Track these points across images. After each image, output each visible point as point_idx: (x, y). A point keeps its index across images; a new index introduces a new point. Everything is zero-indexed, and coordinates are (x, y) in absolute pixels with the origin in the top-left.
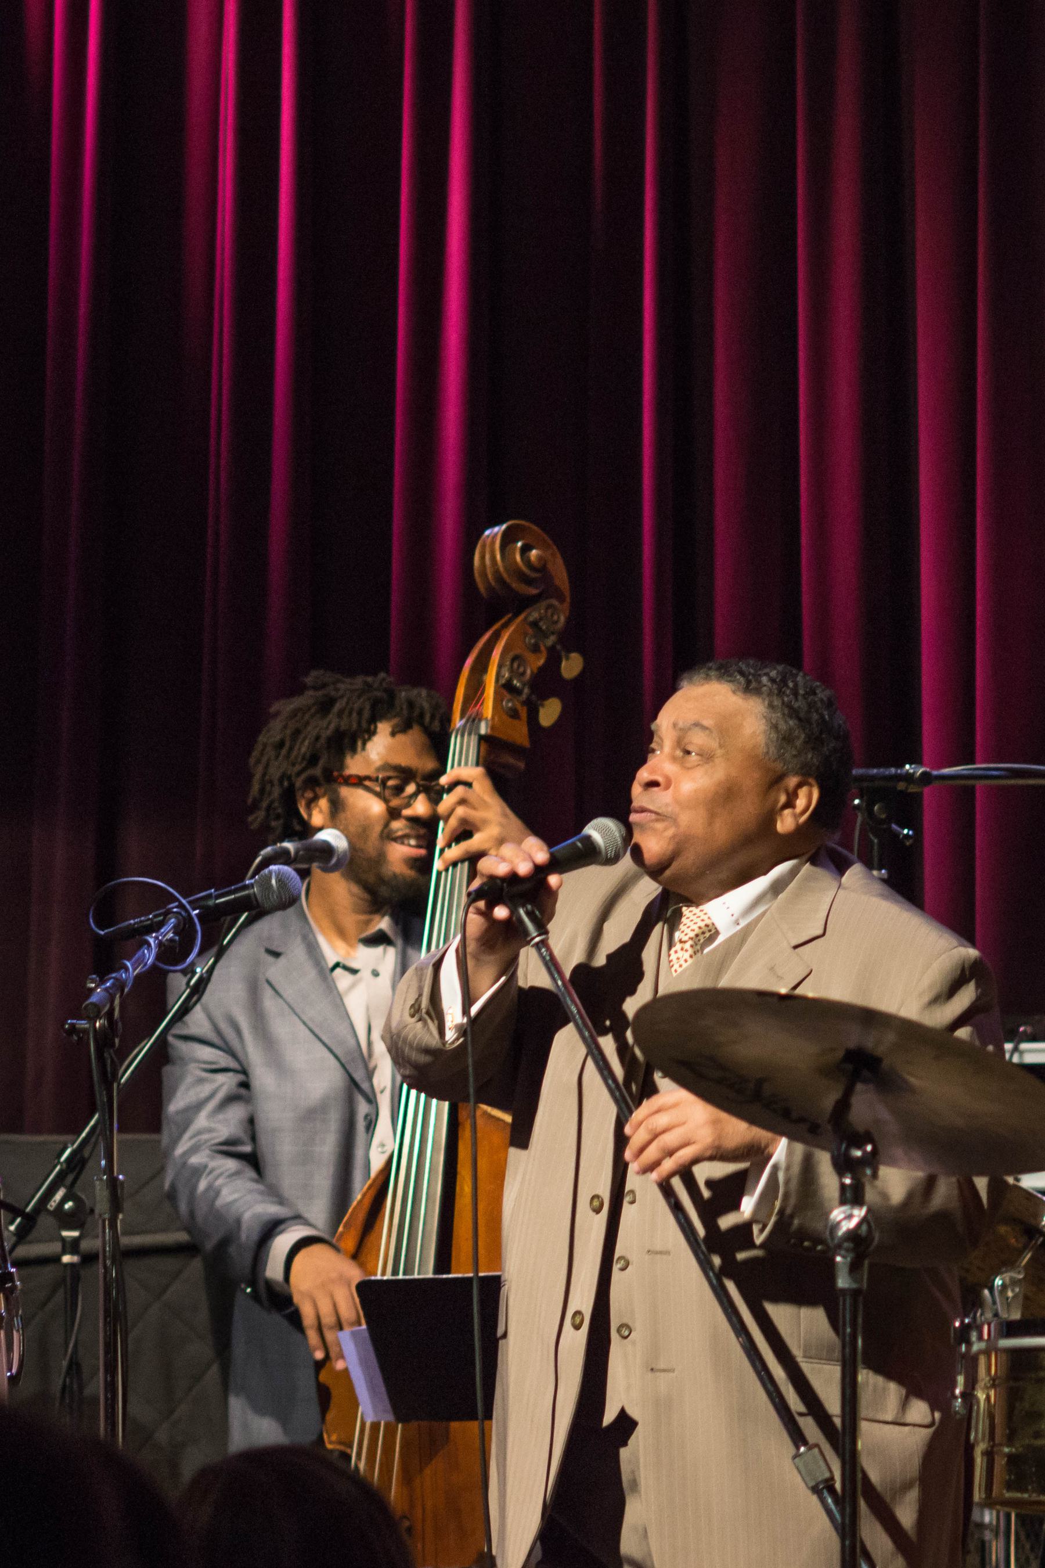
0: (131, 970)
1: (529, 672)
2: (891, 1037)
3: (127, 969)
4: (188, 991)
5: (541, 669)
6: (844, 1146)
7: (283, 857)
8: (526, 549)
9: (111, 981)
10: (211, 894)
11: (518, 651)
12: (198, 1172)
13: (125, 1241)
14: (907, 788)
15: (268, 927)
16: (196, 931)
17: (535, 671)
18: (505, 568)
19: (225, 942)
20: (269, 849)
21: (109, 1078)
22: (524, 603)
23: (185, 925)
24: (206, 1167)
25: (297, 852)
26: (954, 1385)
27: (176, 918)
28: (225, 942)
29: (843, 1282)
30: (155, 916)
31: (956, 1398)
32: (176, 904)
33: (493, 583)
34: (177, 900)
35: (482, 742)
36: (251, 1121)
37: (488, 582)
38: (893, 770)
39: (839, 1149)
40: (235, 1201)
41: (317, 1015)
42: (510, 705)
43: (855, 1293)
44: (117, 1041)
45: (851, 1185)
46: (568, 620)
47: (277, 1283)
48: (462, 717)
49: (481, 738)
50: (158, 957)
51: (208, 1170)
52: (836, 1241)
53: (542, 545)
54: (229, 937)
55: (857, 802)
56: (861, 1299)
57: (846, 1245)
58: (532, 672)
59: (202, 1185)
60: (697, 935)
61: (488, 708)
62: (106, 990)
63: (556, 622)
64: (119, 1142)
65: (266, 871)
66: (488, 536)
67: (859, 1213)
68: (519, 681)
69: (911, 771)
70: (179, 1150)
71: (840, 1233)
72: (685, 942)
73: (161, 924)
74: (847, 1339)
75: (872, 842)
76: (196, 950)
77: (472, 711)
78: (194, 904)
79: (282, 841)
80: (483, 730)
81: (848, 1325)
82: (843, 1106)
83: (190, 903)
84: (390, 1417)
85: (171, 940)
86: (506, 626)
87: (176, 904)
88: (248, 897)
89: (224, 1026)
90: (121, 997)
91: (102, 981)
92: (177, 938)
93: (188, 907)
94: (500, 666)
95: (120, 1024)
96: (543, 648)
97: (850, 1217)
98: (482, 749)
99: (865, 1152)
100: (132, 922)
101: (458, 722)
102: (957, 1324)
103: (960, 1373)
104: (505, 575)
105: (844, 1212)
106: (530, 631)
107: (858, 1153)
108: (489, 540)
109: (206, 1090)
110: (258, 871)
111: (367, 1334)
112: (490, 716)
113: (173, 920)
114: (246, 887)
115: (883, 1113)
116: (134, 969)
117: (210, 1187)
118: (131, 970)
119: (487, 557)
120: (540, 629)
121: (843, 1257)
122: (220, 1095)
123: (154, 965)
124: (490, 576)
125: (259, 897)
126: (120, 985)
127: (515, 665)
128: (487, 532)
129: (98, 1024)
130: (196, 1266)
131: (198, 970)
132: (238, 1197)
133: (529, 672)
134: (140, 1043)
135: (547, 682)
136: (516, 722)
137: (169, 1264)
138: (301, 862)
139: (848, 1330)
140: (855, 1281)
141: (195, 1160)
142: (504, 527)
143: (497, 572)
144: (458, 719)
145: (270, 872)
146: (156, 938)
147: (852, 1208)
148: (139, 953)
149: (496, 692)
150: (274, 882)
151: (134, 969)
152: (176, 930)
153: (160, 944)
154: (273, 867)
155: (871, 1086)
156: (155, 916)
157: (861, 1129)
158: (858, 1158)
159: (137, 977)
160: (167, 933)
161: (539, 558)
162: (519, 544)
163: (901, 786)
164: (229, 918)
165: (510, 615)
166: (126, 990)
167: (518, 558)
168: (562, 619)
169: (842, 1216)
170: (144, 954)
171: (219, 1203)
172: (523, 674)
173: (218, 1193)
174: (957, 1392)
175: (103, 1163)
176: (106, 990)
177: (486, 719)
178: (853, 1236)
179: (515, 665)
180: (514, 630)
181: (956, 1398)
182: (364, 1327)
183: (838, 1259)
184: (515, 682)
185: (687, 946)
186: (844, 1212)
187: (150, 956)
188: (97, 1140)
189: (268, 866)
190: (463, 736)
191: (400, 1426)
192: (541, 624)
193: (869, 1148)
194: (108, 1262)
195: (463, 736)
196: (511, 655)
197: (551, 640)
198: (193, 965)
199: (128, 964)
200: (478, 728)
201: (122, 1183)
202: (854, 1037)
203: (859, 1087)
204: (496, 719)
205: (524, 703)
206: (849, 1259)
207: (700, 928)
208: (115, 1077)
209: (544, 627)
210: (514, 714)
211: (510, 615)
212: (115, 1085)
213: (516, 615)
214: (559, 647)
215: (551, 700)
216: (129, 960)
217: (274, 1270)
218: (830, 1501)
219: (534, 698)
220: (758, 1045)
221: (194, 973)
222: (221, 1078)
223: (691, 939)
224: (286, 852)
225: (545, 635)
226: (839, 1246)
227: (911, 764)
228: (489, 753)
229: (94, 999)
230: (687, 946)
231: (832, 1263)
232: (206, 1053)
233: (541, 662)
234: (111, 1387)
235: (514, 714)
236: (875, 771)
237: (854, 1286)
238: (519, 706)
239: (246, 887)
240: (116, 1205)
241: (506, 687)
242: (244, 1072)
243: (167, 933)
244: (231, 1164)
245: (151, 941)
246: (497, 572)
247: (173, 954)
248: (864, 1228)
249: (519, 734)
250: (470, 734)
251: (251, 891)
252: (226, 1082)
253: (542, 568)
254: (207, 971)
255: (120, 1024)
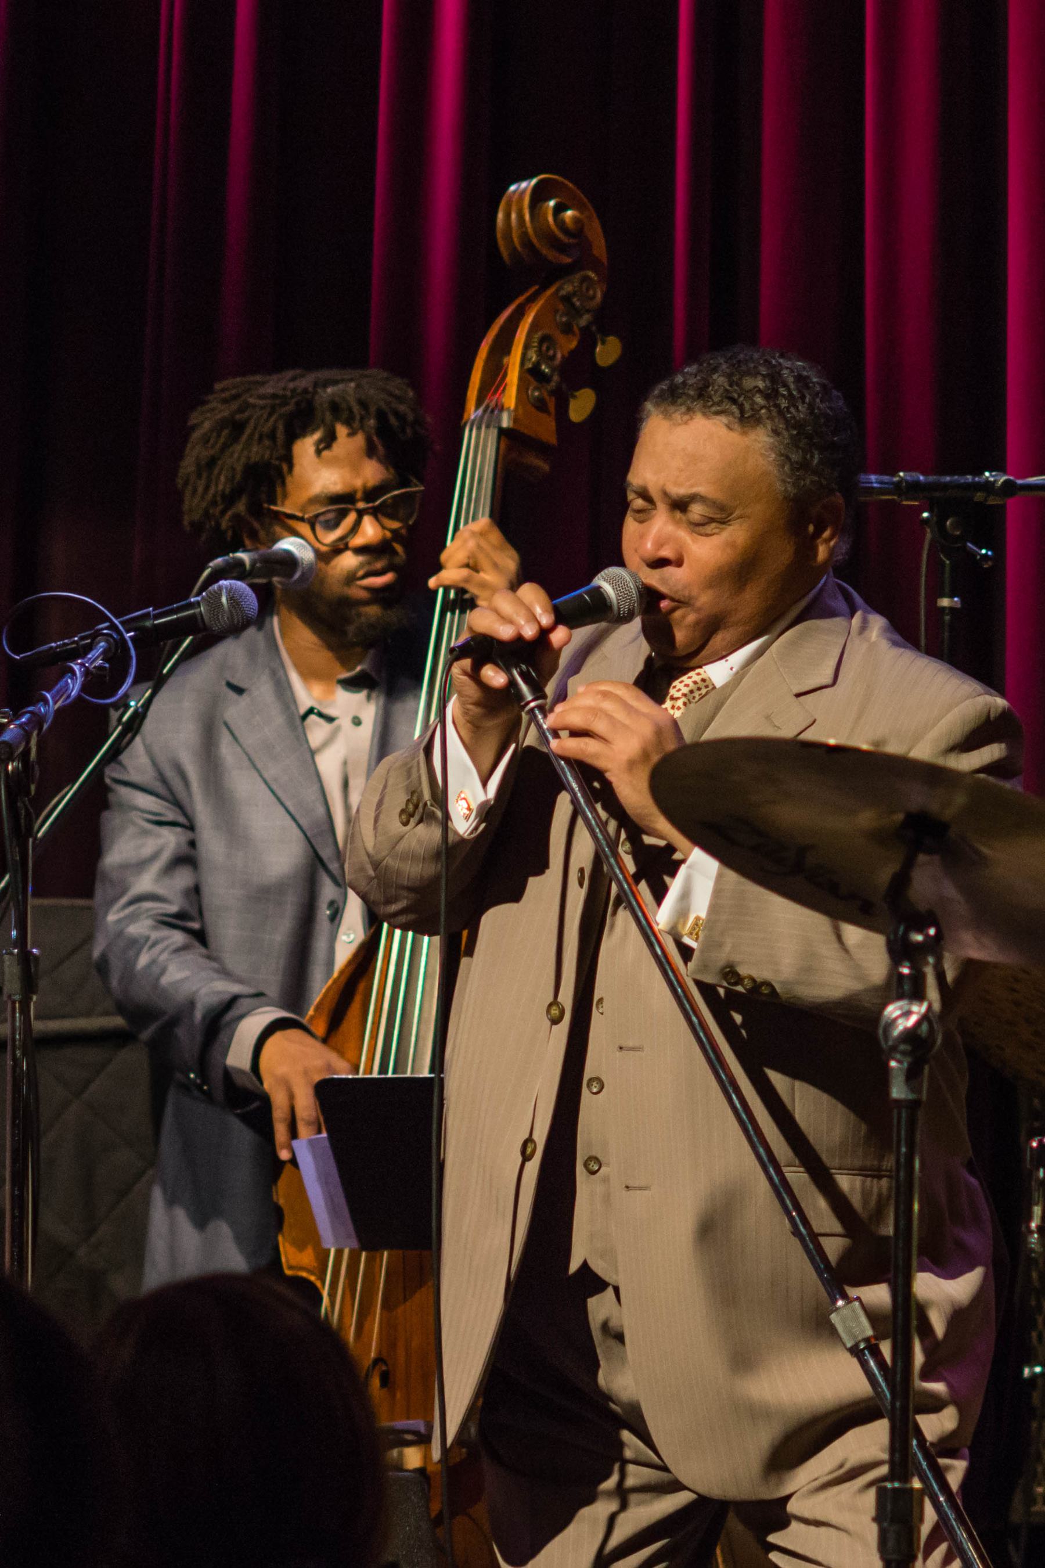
0: (51, 704)
1: (559, 356)
2: (960, 799)
3: (46, 701)
4: (120, 728)
5: (572, 353)
6: (902, 928)
7: (236, 571)
8: (559, 209)
9: (28, 716)
10: (148, 614)
11: (546, 331)
12: (136, 944)
13: (39, 1026)
14: (986, 500)
15: (230, 652)
16: (131, 657)
17: (567, 355)
18: (535, 229)
19: (165, 671)
20: (219, 561)
21: (23, 832)
22: (555, 273)
23: (117, 650)
24: (148, 938)
25: (253, 563)
26: (1030, 1218)
27: (107, 641)
28: (165, 671)
29: (898, 1091)
30: (82, 638)
31: (1032, 1232)
32: (107, 624)
33: (519, 248)
34: (108, 620)
35: (503, 438)
36: (195, 891)
37: (515, 248)
38: (969, 478)
39: (896, 933)
40: (183, 980)
41: (288, 759)
42: (536, 394)
43: (913, 1106)
44: (33, 787)
45: (908, 975)
46: (605, 296)
47: (241, 1072)
48: (477, 407)
49: (502, 432)
50: (84, 688)
51: (149, 943)
52: (890, 1043)
53: (579, 206)
54: (170, 665)
55: (925, 515)
56: (920, 1114)
57: (902, 1047)
58: (563, 357)
59: (143, 960)
60: (691, 692)
61: (510, 397)
62: (21, 726)
63: (594, 297)
64: (33, 907)
65: (215, 586)
66: (515, 192)
67: (918, 1009)
68: (548, 366)
69: (992, 479)
70: (112, 917)
71: (896, 1033)
72: (678, 699)
73: (89, 648)
74: (902, 1160)
75: (943, 564)
76: (129, 680)
77: (491, 401)
78: (128, 625)
79: (235, 551)
80: (505, 423)
81: (903, 1142)
82: (901, 881)
83: (122, 623)
84: (355, 1244)
85: (100, 668)
86: (532, 299)
87: (107, 624)
88: (194, 616)
89: (170, 774)
90: (38, 735)
91: (17, 716)
92: (107, 665)
93: (121, 628)
94: (527, 347)
95: (37, 767)
96: (576, 329)
97: (907, 1014)
98: (503, 446)
99: (927, 936)
100: (53, 644)
101: (472, 412)
102: (1034, 1144)
103: (1037, 1204)
104: (535, 241)
105: (901, 1008)
106: (561, 307)
107: (919, 938)
108: (516, 196)
109: (149, 847)
110: (205, 587)
111: (327, 1144)
112: (512, 406)
113: (102, 644)
114: (191, 606)
115: (950, 890)
116: (55, 703)
117: (153, 962)
118: (51, 704)
119: (514, 216)
120: (573, 305)
121: (898, 1061)
122: (166, 856)
123: (79, 697)
124: (516, 240)
125: (206, 618)
126: (38, 720)
127: (544, 348)
128: (513, 188)
129: (10, 767)
130: (134, 1059)
131: (132, 703)
132: (183, 977)
133: (559, 356)
134: (63, 788)
135: (579, 369)
136: (543, 416)
137: (92, 1054)
138: (259, 577)
139: (904, 1150)
140: (912, 1090)
141: (134, 929)
142: (534, 181)
143: (524, 235)
144: (473, 409)
145: (220, 588)
146: (82, 665)
147: (911, 1003)
148: (61, 684)
149: (521, 379)
150: (224, 600)
151: (55, 703)
152: (106, 655)
153: (87, 673)
154: (223, 582)
155: (936, 858)
156: (82, 638)
157: (922, 907)
158: (919, 943)
159: (58, 712)
160: (95, 658)
161: (576, 220)
162: (552, 203)
163: (979, 496)
164: (170, 642)
165: (537, 287)
166: (45, 727)
167: (550, 219)
168: (599, 294)
169: (898, 1013)
170: (67, 684)
171: (164, 980)
172: (554, 357)
173: (163, 971)
174: (1033, 1225)
175: (14, 933)
176: (21, 726)
177: (508, 409)
178: (910, 1035)
179: (544, 348)
180: (543, 307)
181: (1032, 1232)
182: (324, 1135)
183: (893, 1063)
184: (543, 367)
185: (680, 703)
186: (901, 1008)
187: (74, 687)
188: (8, 904)
189: (217, 581)
190: (479, 428)
191: (364, 1254)
192: (575, 300)
193: (932, 931)
194: (18, 1053)
195: (479, 428)
196: (537, 336)
197: (585, 320)
198: (126, 696)
199: (48, 696)
200: (500, 421)
201: (36, 958)
202: (916, 797)
203: (922, 858)
204: (520, 411)
205: (552, 393)
206: (906, 1065)
207: (695, 683)
208: (30, 832)
209: (578, 304)
210: (540, 405)
211: (537, 287)
212: (31, 840)
213: (544, 288)
214: (594, 328)
215: (583, 391)
216: (48, 691)
217: (238, 1056)
218: (872, 1363)
219: (564, 387)
220: (800, 812)
221: (127, 707)
222: (165, 831)
223: (685, 695)
224: (240, 563)
225: (578, 313)
226: (894, 1048)
227: (991, 471)
228: (509, 449)
229: (6, 737)
230: (680, 703)
231: (886, 1069)
232: (143, 800)
233: (573, 344)
234: (19, 1202)
235: (540, 405)
236: (948, 479)
237: (911, 1096)
238: (546, 395)
239: (191, 606)
240: (29, 984)
241: (532, 374)
242: (191, 827)
243: (95, 658)
244: (178, 938)
245: (76, 668)
246: (524, 235)
247: (101, 683)
248: (925, 1027)
249: (546, 429)
250: (488, 427)
251: (197, 610)
252: (170, 840)
253: (578, 231)
254: (143, 706)
255: (37, 767)
